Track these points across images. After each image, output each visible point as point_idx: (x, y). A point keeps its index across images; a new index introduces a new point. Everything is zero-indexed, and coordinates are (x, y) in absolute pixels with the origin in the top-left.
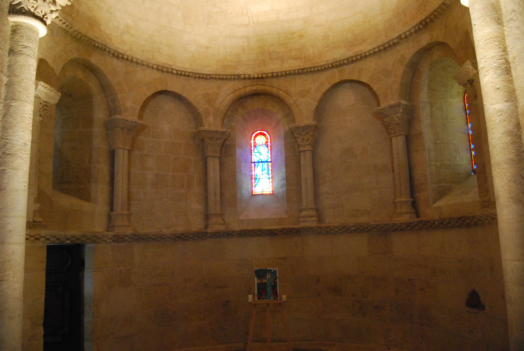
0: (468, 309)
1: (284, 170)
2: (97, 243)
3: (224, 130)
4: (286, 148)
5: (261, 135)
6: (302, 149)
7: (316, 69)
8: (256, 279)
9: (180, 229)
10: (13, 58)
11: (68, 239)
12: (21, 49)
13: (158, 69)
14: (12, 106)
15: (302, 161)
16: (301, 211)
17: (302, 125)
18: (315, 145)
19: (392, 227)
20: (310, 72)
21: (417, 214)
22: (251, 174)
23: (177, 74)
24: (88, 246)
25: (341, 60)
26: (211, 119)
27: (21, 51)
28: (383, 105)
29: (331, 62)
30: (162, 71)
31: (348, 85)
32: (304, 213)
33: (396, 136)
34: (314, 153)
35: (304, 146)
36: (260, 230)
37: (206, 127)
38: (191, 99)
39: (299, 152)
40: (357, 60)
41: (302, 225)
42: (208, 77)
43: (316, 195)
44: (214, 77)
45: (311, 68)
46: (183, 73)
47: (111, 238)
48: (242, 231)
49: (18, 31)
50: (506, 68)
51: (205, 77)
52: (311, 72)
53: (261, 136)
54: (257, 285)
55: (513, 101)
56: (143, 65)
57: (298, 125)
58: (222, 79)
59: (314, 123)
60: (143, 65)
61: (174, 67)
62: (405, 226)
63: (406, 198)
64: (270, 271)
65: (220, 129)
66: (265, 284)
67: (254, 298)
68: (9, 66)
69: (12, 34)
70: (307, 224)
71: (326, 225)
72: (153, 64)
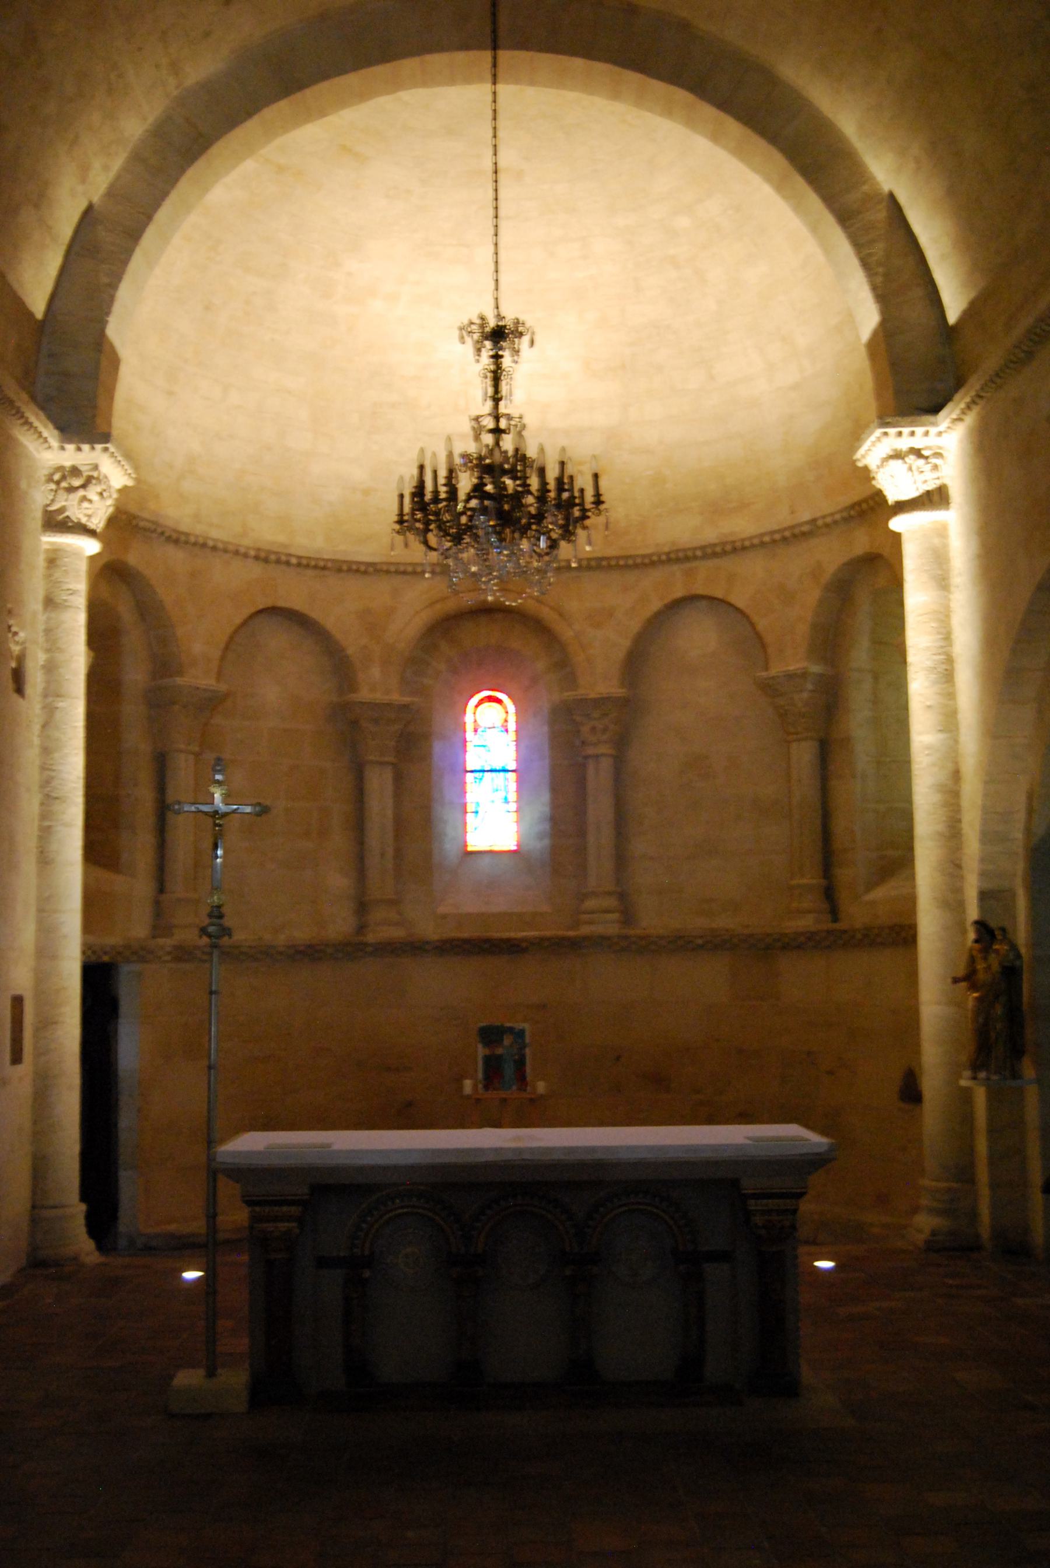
0: (902, 1105)
1: (546, 797)
2: (146, 962)
3: (407, 699)
4: (552, 748)
5: (490, 701)
6: (591, 751)
7: (630, 562)
8: (480, 1046)
9: (302, 935)
10: (53, 615)
11: (105, 953)
12: (65, 598)
13: (257, 558)
14: (57, 708)
15: (591, 785)
16: (583, 897)
17: (592, 696)
18: (622, 743)
19: (779, 940)
20: (615, 566)
21: (834, 913)
22: (463, 801)
23: (299, 565)
24: (126, 971)
25: (689, 549)
26: (376, 672)
27: (65, 601)
28: (774, 672)
29: (666, 549)
30: (266, 560)
31: (704, 603)
32: (590, 904)
33: (799, 740)
34: (619, 762)
35: (595, 745)
36: (488, 940)
37: (364, 694)
38: (329, 622)
39: (586, 757)
40: (725, 553)
41: (585, 930)
42: (371, 569)
43: (621, 860)
44: (385, 568)
45: (618, 558)
46: (313, 563)
47: (169, 953)
48: (445, 942)
49: (58, 562)
50: (946, 670)
51: (363, 568)
52: (618, 567)
53: (490, 706)
54: (405, 1145)
55: (950, 731)
56: (225, 551)
57: (582, 695)
58: (404, 573)
59: (618, 691)
60: (225, 551)
61: (292, 551)
62: (802, 939)
63: (811, 879)
64: (511, 1030)
65: (396, 698)
66: (500, 1057)
67: (475, 1087)
68: (48, 631)
69: (48, 568)
70: (598, 929)
71: (638, 932)
72: (248, 548)
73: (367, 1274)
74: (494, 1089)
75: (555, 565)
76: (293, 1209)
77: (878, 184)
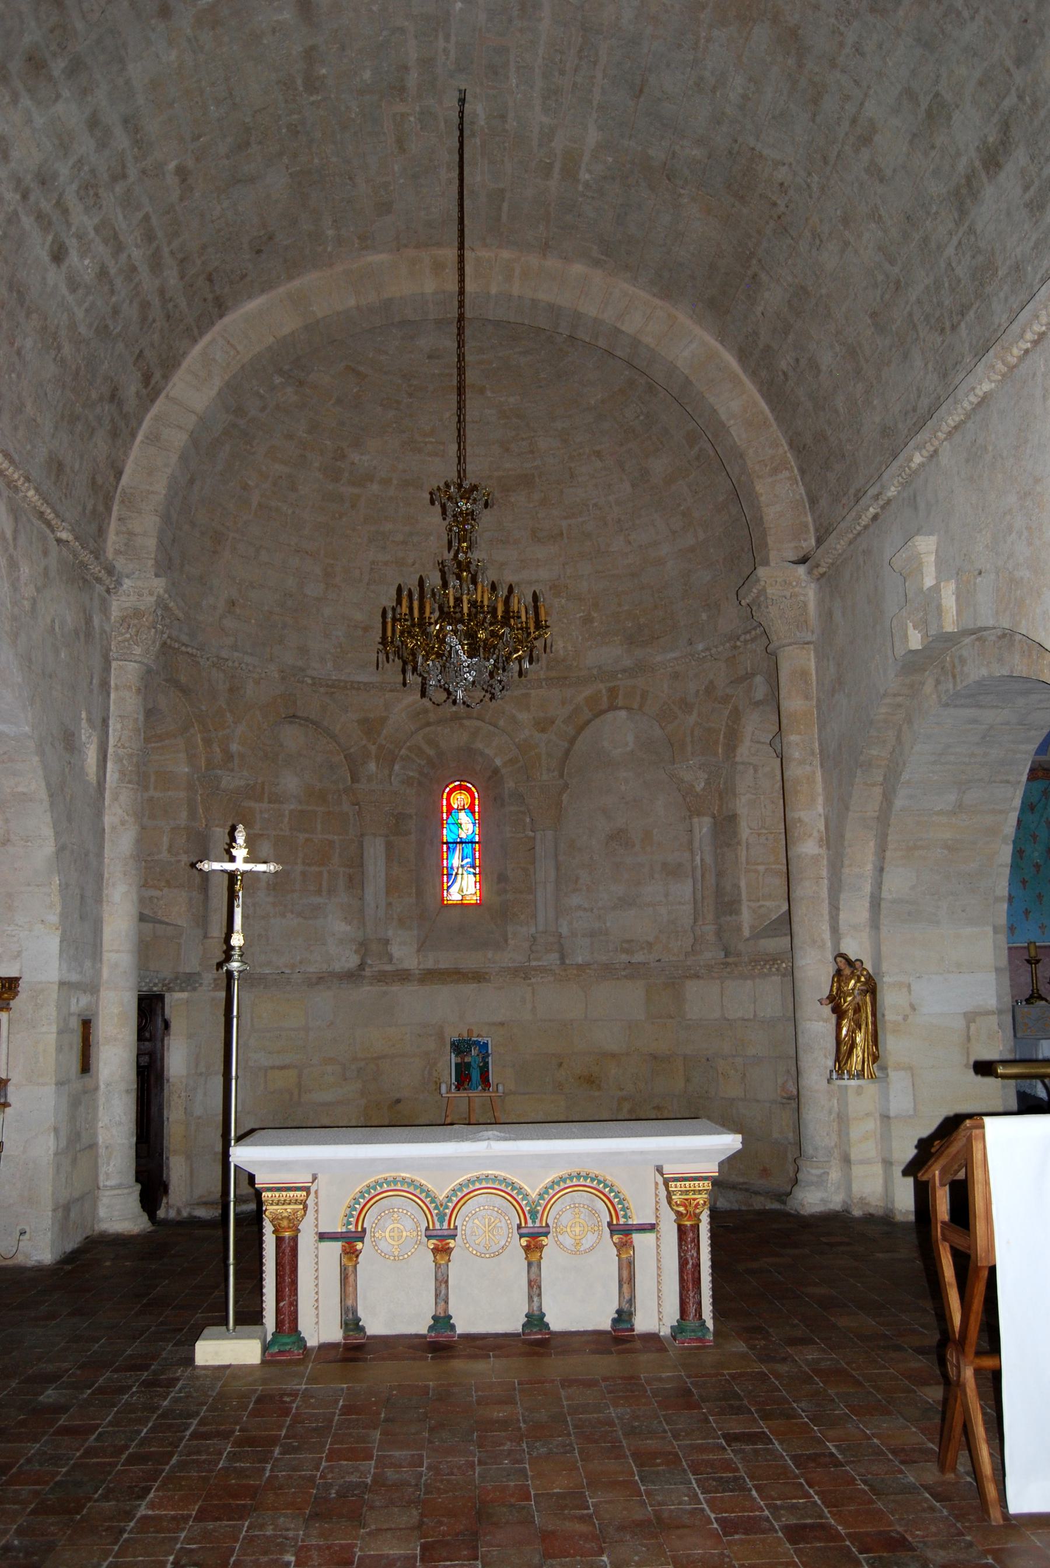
73: (359, 1245)
74: (465, 1089)
75: (1029, 268)
76: (298, 1193)
77: (95, 1119)
